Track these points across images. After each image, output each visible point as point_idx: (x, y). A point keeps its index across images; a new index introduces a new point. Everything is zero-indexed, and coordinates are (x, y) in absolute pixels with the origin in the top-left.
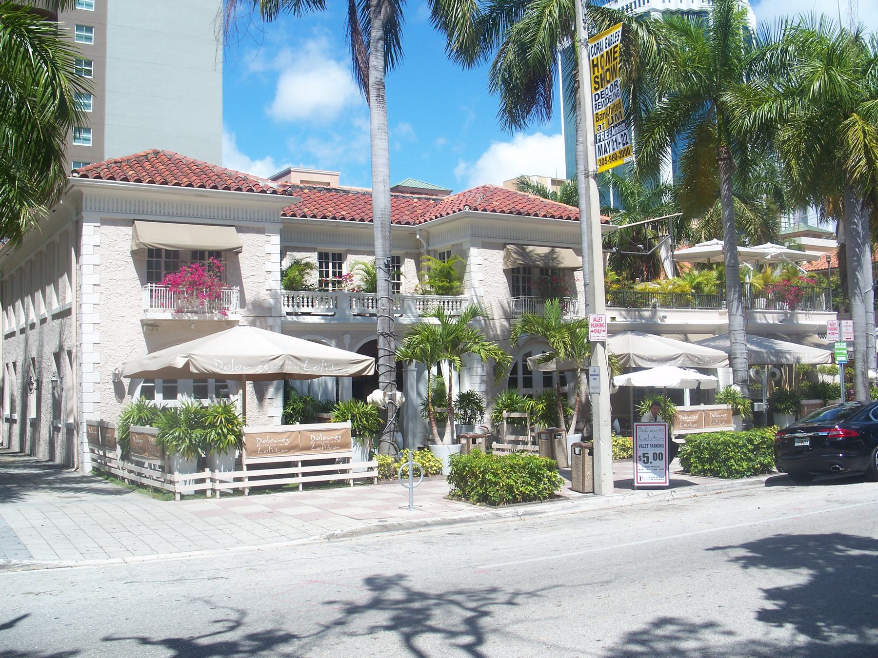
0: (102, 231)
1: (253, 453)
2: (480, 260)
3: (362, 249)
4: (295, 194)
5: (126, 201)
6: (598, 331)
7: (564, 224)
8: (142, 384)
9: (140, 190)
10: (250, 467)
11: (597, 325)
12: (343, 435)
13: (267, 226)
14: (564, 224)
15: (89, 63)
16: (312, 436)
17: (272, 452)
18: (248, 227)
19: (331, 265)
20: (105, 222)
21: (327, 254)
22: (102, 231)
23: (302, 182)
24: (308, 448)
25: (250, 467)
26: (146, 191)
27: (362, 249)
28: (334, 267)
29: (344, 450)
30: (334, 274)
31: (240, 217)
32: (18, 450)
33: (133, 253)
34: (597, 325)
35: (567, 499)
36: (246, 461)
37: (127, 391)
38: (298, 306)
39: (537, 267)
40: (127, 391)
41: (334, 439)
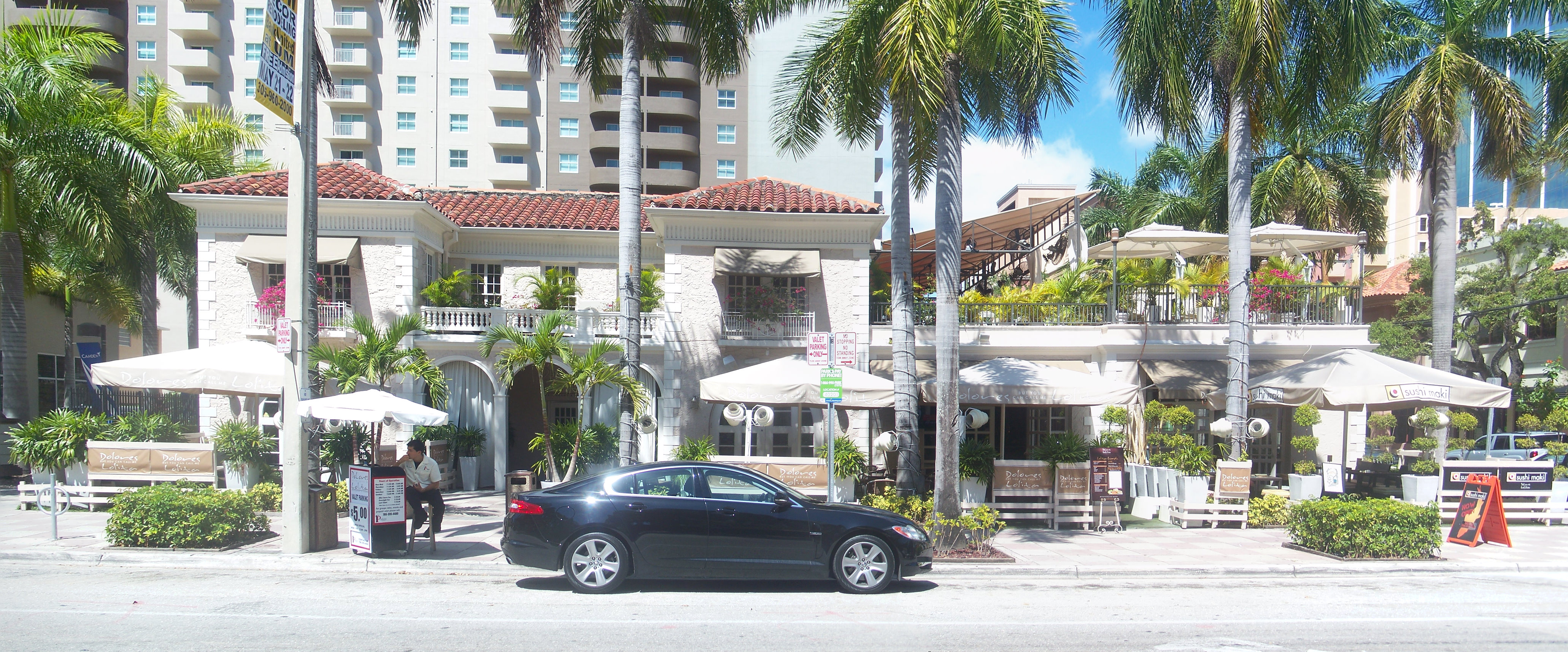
0: (217, 247)
1: (98, 468)
2: (677, 268)
3: (596, 261)
4: (763, 208)
5: (263, 216)
6: (818, 354)
7: (801, 219)
8: (265, 401)
9: (246, 203)
10: (97, 483)
11: (817, 347)
12: (201, 458)
13: (397, 236)
14: (801, 219)
15: (731, 94)
16: (165, 455)
17: (119, 468)
18: (375, 238)
19: (486, 278)
20: (219, 238)
21: (481, 267)
22: (217, 247)
23: (497, 184)
24: (161, 469)
25: (97, 483)
26: (251, 203)
27: (596, 261)
28: (490, 281)
29: (207, 474)
30: (490, 289)
31: (736, 238)
32: (1326, 490)
33: (717, 281)
34: (817, 347)
35: (1005, 558)
36: (92, 476)
37: (242, 407)
38: (443, 324)
39: (768, 275)
40: (242, 407)
41: (190, 461)
